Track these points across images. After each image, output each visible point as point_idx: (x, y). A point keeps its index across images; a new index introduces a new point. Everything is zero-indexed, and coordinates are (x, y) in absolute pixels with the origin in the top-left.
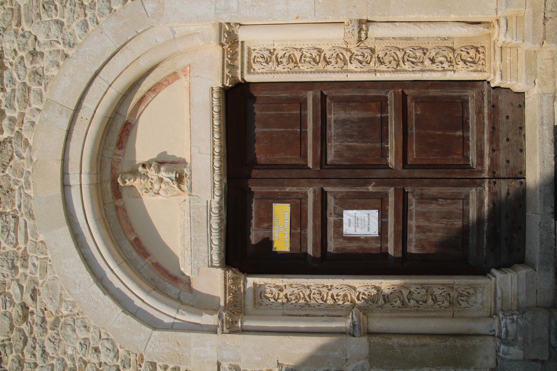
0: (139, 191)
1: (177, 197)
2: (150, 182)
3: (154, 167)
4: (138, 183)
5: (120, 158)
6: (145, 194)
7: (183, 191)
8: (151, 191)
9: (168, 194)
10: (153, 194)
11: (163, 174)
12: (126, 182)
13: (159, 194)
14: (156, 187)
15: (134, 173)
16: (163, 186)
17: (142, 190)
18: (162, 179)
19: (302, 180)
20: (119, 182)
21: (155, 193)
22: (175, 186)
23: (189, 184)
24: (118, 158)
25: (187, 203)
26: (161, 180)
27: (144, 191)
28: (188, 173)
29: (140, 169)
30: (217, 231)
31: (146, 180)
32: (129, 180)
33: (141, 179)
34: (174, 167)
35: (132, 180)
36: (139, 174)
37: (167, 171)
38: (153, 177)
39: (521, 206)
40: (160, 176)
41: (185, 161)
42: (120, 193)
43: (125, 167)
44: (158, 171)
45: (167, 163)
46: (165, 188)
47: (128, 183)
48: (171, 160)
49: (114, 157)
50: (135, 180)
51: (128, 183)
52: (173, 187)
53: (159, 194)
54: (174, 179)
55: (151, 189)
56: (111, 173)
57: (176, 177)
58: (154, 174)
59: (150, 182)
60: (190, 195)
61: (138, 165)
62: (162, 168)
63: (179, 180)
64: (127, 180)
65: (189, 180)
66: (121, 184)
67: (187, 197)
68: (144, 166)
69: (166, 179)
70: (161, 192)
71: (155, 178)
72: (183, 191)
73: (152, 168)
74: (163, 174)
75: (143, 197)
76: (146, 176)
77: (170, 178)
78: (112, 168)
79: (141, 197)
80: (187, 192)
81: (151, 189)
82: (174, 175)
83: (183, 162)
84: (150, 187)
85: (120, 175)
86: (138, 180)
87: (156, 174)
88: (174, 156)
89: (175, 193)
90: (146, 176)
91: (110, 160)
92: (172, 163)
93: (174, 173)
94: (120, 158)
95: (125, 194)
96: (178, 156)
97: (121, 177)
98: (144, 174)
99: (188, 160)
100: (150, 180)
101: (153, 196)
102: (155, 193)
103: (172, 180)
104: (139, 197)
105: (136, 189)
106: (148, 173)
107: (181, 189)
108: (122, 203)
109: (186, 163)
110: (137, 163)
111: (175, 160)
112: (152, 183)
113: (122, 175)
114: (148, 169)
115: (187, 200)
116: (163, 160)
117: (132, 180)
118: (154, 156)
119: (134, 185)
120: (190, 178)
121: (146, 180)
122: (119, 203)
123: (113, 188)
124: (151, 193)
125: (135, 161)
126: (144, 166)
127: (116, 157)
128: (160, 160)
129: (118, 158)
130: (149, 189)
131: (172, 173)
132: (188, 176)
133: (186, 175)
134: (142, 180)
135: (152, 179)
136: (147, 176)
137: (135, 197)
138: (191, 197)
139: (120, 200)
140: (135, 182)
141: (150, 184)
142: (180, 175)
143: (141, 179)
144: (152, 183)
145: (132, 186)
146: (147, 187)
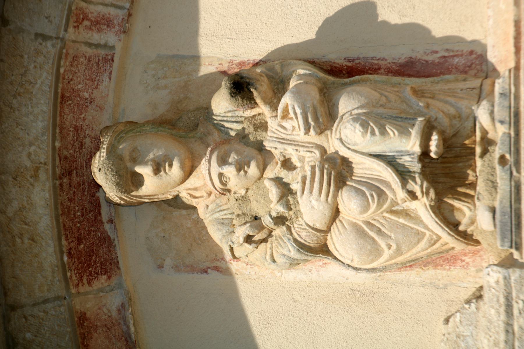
0: (216, 234)
1: (430, 273)
2: (278, 181)
3: (298, 93)
4: (205, 187)
5: (110, 37)
6: (243, 250)
7: (466, 237)
8: (279, 231)
9: (377, 252)
10: (294, 253)
11: (350, 138)
12: (137, 181)
13: (323, 250)
14: (311, 209)
15: (187, 128)
16: (349, 203)
17: (228, 226)
18: (346, 163)
19: (216, 186)
20: (100, 178)
21: (302, 247)
22: (422, 207)
23: (501, 198)
24: (96, 37)
25: (491, 311)
26: (338, 171)
27: (241, 232)
28: (499, 132)
29: (221, 104)
30: (114, 314)
31: (253, 170)
32: (157, 170)
33: (223, 161)
34: (418, 93)
35: (175, 171)
36: (216, 136)
37: (374, 119)
38: (291, 152)
39: (356, 226)
40: (333, 145)
41: (482, 58)
42: (107, 242)
43: (138, 96)
44: (324, 116)
45: (375, 70)
46: (360, 219)
47: (152, 185)
48: (399, 53)
49: (71, 34)
50: (188, 172)
51: (152, 185)
52: (406, 213)
53: (323, 250)
54: (416, 167)
55: (280, 220)
56: (57, 127)
57: (425, 154)
58: (300, 135)
59: (278, 181)
60: (508, 263)
61: (211, 84)
62: (347, 104)
63: (446, 172)
64: (145, 171)
65: (501, 175)
66: (112, 192)
67: (493, 277)
68: (241, 87)
69: (366, 168)
70: (337, 241)
71: (306, 160)
72: (466, 237)
73: (287, 99)
74: (350, 138)
75: (234, 266)
76: (250, 148)
77: (390, 161)
78: (62, 98)
79: (227, 272)
80: (492, 247)
81: (280, 220)
82: (412, 144)
83: (469, 65)
84: (278, 209)
85: (106, 141)
86: (207, 171)
87: (313, 137)
88: (416, 31)
89: (420, 249)
90: (250, 148)
91: (50, 48)
92: (407, 69)
93: (415, 133)
94: (110, 37)
95: (131, 245)
96: (439, 30)
97: (112, 151)
98: (242, 136)
99: (500, 55)
100: (274, 170)
101: (293, 263)
102: (302, 247)
103: (403, 174)
104: (214, 265)
105: (199, 224)
106: (263, 126)
107: (453, 225)
108: (113, 301)
109: (488, 72)
110: (206, 69)
111: (419, 52)
112: (285, 191)
113: (118, 139)
114: (263, 109)
115: (493, 297)
116: (353, 54)
117: (175, 171)
118: (302, 31)
119: (184, 195)
120: (512, 162)
121: (253, 170)
122: (99, 299)
123: (62, 211)
124: (283, 246)
125: (196, 58)
126: (241, 87)
127: (84, 35)
128: (336, 55)
129: (96, 37)
130: (267, 221)
131: (404, 132)
132: (497, 152)
133: (487, 143)
134: (230, 171)
135: (287, 164)
136: (260, 147)
137: (192, 269)
138: (515, 274)
139: (102, 281)
140: (193, 181)
141: (274, 192)
142: (446, 143)
143: (223, 161)
144: (285, 191)
145: (176, 202)
146: (256, 207)
